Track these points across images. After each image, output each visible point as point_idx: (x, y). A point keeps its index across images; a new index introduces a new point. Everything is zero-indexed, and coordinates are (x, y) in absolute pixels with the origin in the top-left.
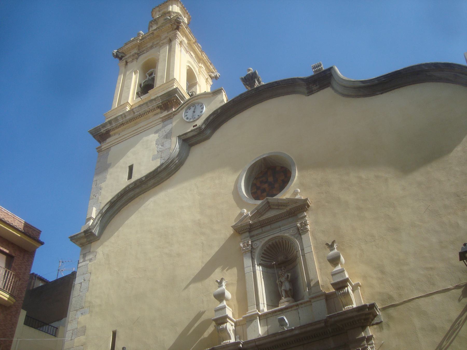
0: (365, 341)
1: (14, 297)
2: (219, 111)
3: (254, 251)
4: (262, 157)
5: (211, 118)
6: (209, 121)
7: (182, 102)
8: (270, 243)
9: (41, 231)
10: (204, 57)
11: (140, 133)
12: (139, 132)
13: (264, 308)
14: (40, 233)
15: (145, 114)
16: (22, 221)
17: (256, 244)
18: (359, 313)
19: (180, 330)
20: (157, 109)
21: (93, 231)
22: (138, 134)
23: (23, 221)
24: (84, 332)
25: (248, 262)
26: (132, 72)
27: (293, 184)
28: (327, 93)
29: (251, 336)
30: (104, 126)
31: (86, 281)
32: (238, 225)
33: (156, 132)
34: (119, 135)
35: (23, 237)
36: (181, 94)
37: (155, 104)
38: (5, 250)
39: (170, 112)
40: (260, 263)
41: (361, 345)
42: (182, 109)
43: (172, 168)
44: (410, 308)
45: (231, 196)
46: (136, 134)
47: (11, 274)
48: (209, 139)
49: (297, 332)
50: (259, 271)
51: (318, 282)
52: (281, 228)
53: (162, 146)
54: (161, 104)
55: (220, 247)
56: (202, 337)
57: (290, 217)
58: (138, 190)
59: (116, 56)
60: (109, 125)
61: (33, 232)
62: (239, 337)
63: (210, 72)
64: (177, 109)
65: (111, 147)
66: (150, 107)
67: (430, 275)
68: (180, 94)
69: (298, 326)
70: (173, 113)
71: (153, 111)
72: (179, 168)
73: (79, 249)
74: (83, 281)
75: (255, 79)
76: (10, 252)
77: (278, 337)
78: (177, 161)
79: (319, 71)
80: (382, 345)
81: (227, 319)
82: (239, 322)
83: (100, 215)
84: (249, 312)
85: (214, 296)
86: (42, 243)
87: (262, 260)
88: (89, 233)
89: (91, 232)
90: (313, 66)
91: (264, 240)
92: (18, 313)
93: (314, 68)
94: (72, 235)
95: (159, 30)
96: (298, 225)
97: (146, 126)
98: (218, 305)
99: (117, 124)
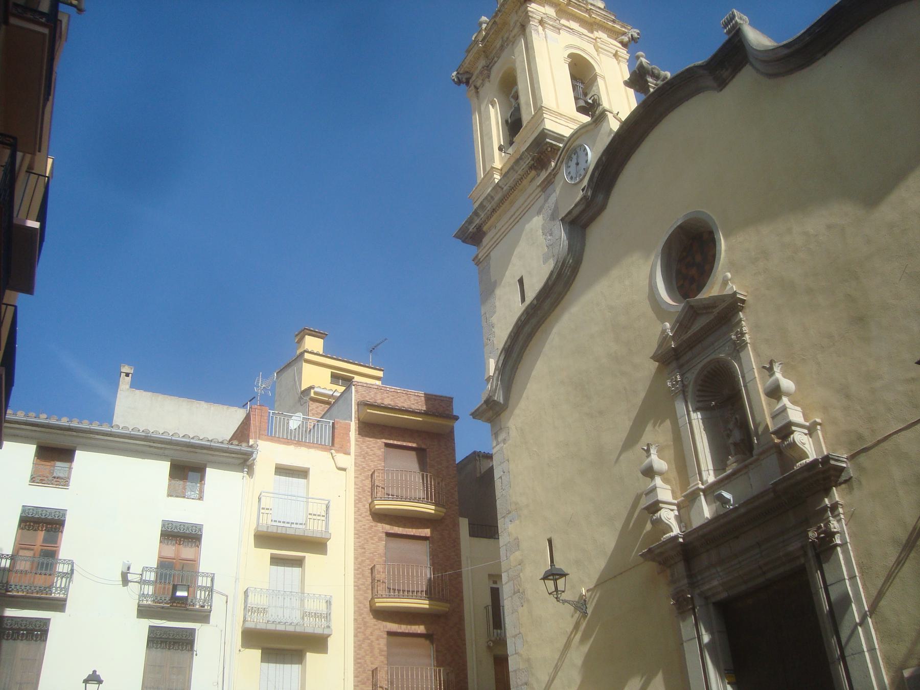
0: (829, 512)
1: (443, 506)
2: (604, 158)
3: (687, 389)
4: (675, 227)
5: (596, 174)
6: (595, 180)
7: (561, 145)
9: (452, 398)
10: (596, 18)
11: (520, 218)
16: (420, 395)
17: (686, 378)
19: (619, 525)
20: (530, 172)
21: (496, 399)
23: (421, 394)
24: (518, 546)
26: (487, 106)
27: (720, 265)
28: (746, 78)
29: (696, 523)
30: (470, 221)
31: (505, 473)
32: (659, 354)
33: (539, 213)
35: (426, 420)
36: (556, 135)
37: (524, 165)
38: (410, 444)
41: (824, 518)
43: (567, 274)
44: (887, 451)
47: (427, 477)
48: (605, 208)
49: (742, 510)
50: (696, 421)
51: (767, 426)
53: (551, 235)
54: (533, 162)
56: (645, 531)
59: (459, 82)
60: (476, 218)
61: (440, 404)
62: (684, 525)
63: (619, 36)
65: (491, 253)
67: (912, 391)
69: (742, 502)
72: (578, 271)
73: (488, 426)
74: (502, 473)
75: (646, 76)
76: (417, 444)
79: (733, 30)
81: (660, 504)
83: (497, 372)
84: (691, 486)
85: (642, 473)
87: (698, 401)
90: (724, 23)
92: (456, 525)
93: (726, 25)
95: (501, 14)
96: (733, 337)
98: (649, 485)
99: (486, 214)
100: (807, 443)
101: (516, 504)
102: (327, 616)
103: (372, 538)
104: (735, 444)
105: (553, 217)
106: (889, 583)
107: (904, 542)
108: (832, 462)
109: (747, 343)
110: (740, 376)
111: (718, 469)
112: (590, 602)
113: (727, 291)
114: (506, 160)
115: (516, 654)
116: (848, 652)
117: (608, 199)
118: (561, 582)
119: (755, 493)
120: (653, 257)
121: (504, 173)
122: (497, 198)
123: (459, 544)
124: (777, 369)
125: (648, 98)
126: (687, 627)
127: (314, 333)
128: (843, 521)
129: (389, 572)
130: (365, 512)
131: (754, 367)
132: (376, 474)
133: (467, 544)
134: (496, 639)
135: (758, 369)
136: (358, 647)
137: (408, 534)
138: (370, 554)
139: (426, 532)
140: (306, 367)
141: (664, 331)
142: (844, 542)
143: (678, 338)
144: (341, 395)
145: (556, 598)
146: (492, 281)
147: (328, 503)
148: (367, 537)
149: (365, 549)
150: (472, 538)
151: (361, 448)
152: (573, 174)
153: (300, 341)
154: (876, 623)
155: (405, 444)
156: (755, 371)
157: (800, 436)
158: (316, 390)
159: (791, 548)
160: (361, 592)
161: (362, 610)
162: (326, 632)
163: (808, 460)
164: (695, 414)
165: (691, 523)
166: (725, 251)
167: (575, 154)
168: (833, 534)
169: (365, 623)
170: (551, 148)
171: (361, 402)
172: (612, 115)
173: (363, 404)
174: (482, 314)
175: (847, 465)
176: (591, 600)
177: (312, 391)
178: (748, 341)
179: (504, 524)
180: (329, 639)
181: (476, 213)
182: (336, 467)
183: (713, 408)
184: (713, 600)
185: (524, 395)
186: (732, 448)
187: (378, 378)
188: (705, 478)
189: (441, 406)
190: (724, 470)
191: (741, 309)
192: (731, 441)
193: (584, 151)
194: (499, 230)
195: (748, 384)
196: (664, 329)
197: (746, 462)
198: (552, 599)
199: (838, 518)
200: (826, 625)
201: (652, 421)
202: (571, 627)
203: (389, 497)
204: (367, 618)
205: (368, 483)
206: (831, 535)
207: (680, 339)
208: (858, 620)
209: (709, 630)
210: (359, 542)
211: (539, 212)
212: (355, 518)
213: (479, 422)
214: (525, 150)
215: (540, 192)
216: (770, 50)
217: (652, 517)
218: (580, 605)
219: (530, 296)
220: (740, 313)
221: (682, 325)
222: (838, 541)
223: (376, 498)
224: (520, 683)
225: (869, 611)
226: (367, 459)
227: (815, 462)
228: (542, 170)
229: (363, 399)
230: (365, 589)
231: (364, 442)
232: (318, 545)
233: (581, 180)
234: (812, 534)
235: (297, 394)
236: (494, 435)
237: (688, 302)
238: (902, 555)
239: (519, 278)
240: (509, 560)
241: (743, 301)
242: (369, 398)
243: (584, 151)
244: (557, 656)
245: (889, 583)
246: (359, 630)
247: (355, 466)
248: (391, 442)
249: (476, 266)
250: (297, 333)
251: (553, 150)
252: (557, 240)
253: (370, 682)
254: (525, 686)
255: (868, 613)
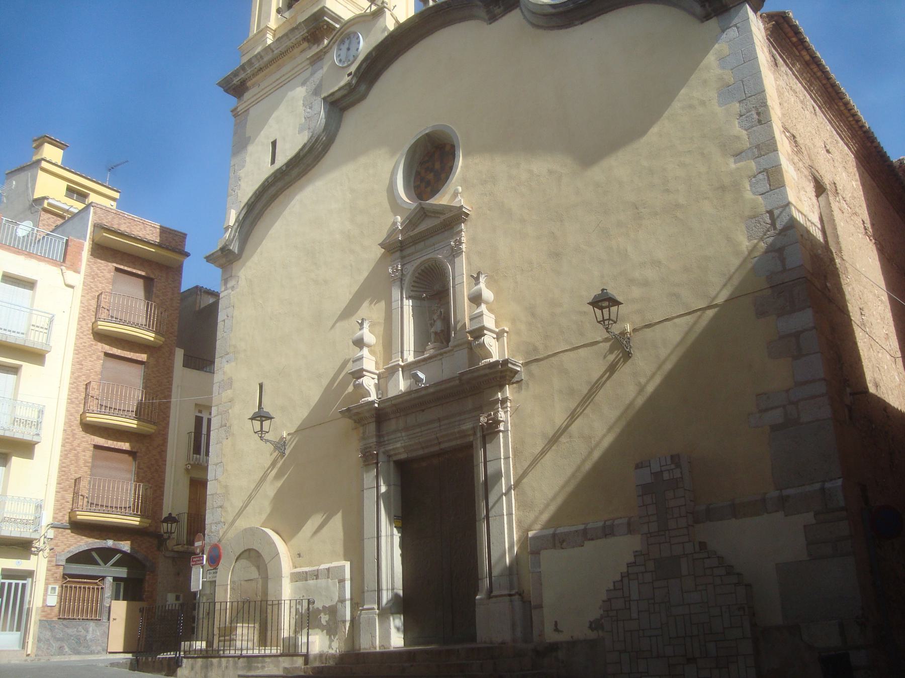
1: (163, 336)
2: (374, 53)
3: (404, 278)
5: (364, 66)
6: (362, 70)
7: (338, 26)
8: (423, 268)
9: (186, 235)
11: (284, 84)
12: (282, 84)
13: (410, 357)
14: (186, 238)
15: (289, 51)
16: (156, 226)
18: (491, 371)
19: (325, 382)
20: (303, 43)
21: (231, 248)
22: (281, 87)
25: (396, 293)
29: (392, 393)
30: (235, 74)
32: (387, 243)
34: (259, 87)
37: (299, 35)
38: (139, 272)
39: (321, 47)
40: (410, 295)
42: (334, 43)
43: (318, 149)
45: (385, 194)
46: (278, 87)
48: (366, 98)
49: (432, 390)
52: (436, 246)
53: (310, 108)
55: (369, 271)
56: (347, 392)
57: (446, 230)
58: (280, 184)
64: (330, 38)
66: (293, 40)
68: (331, 16)
70: (324, 51)
71: (299, 46)
73: (219, 271)
76: (147, 273)
77: (413, 396)
78: (324, 138)
80: (518, 408)
82: (383, 373)
83: (237, 224)
84: (392, 361)
86: (187, 255)
87: (412, 291)
88: (227, 252)
89: (229, 250)
91: (416, 263)
92: (172, 354)
94: (207, 255)
96: (452, 243)
97: (290, 74)
98: (357, 354)
99: (253, 70)
100: (494, 346)
101: (235, 347)
102: (38, 424)
103: (90, 356)
104: (436, 333)
105: (316, 92)
106: (533, 466)
107: (550, 437)
108: (510, 365)
109: (463, 251)
110: (451, 278)
111: (419, 350)
112: (289, 444)
113: (455, 203)
114: (281, 23)
115: (215, 480)
116: (491, 514)
117: (370, 91)
118: (266, 424)
119: (444, 378)
120: (398, 155)
121: (277, 37)
122: (266, 59)
123: (172, 372)
124: (482, 279)
125: (425, 10)
126: (369, 478)
127: (55, 142)
128: (509, 413)
129: (103, 390)
130: (88, 331)
131: (464, 273)
132: (103, 296)
133: (181, 374)
134: (195, 463)
135: (467, 275)
136: (64, 456)
137: (126, 356)
138: (87, 370)
139: (143, 357)
140: (41, 175)
141: (395, 223)
142: (506, 430)
143: (405, 232)
144: (78, 213)
145: (261, 437)
146: (247, 136)
147: (52, 317)
148: (87, 354)
149: (82, 365)
150: (185, 368)
151: (91, 268)
152: (343, 57)
153: (38, 148)
154: (517, 495)
155: (134, 271)
156: (465, 276)
157: (489, 339)
158: (50, 201)
159: (464, 427)
160: (74, 406)
161: (72, 422)
162: (35, 439)
163: (492, 360)
164: (407, 301)
165: (387, 393)
166: (461, 167)
167: (348, 39)
168: (499, 422)
169: (74, 435)
170: (327, 26)
171: (98, 224)
172: (390, 12)
173: (98, 227)
174: (232, 165)
175: (521, 370)
176: (290, 443)
177: (46, 202)
178: (464, 250)
179: (221, 364)
180: (36, 446)
181: (243, 68)
182: (65, 284)
183: (424, 299)
184: (395, 458)
185: (259, 250)
186: (433, 336)
187: (114, 199)
188: (405, 357)
189: (174, 240)
190: (423, 352)
191: (464, 221)
192: (433, 330)
193: (357, 39)
194: (263, 89)
195: (456, 286)
196: (395, 221)
197: (442, 351)
198: (256, 436)
199: (506, 410)
200: (480, 491)
201: (369, 299)
202: (269, 463)
203: (113, 319)
204: (76, 430)
205: (94, 303)
206: (497, 422)
207: (407, 234)
208: (504, 491)
209: (388, 485)
210: (78, 358)
211: (303, 84)
212: (77, 335)
213: (211, 266)
214: (303, 22)
215: (308, 64)
216: (539, 4)
217: (355, 381)
218: (280, 446)
219: (281, 160)
220: (463, 224)
221: (412, 222)
222: (502, 428)
223: (100, 318)
224: (215, 506)
225: (514, 485)
226: (96, 280)
227: (497, 362)
228: (314, 44)
229: (100, 222)
230: (78, 402)
231: (95, 263)
232: (36, 356)
233: (349, 66)
234: (483, 419)
235: (29, 201)
236: (223, 281)
237: (420, 203)
238: (547, 447)
239: (272, 141)
240: (220, 397)
241: (467, 215)
242: (106, 222)
243: (357, 39)
244: (253, 486)
245: (533, 466)
246: (67, 440)
247: (84, 285)
248: (122, 267)
249: (233, 118)
250: (35, 138)
251: (328, 28)
252: (315, 114)
253: (72, 489)
254: (220, 509)
255: (513, 486)
